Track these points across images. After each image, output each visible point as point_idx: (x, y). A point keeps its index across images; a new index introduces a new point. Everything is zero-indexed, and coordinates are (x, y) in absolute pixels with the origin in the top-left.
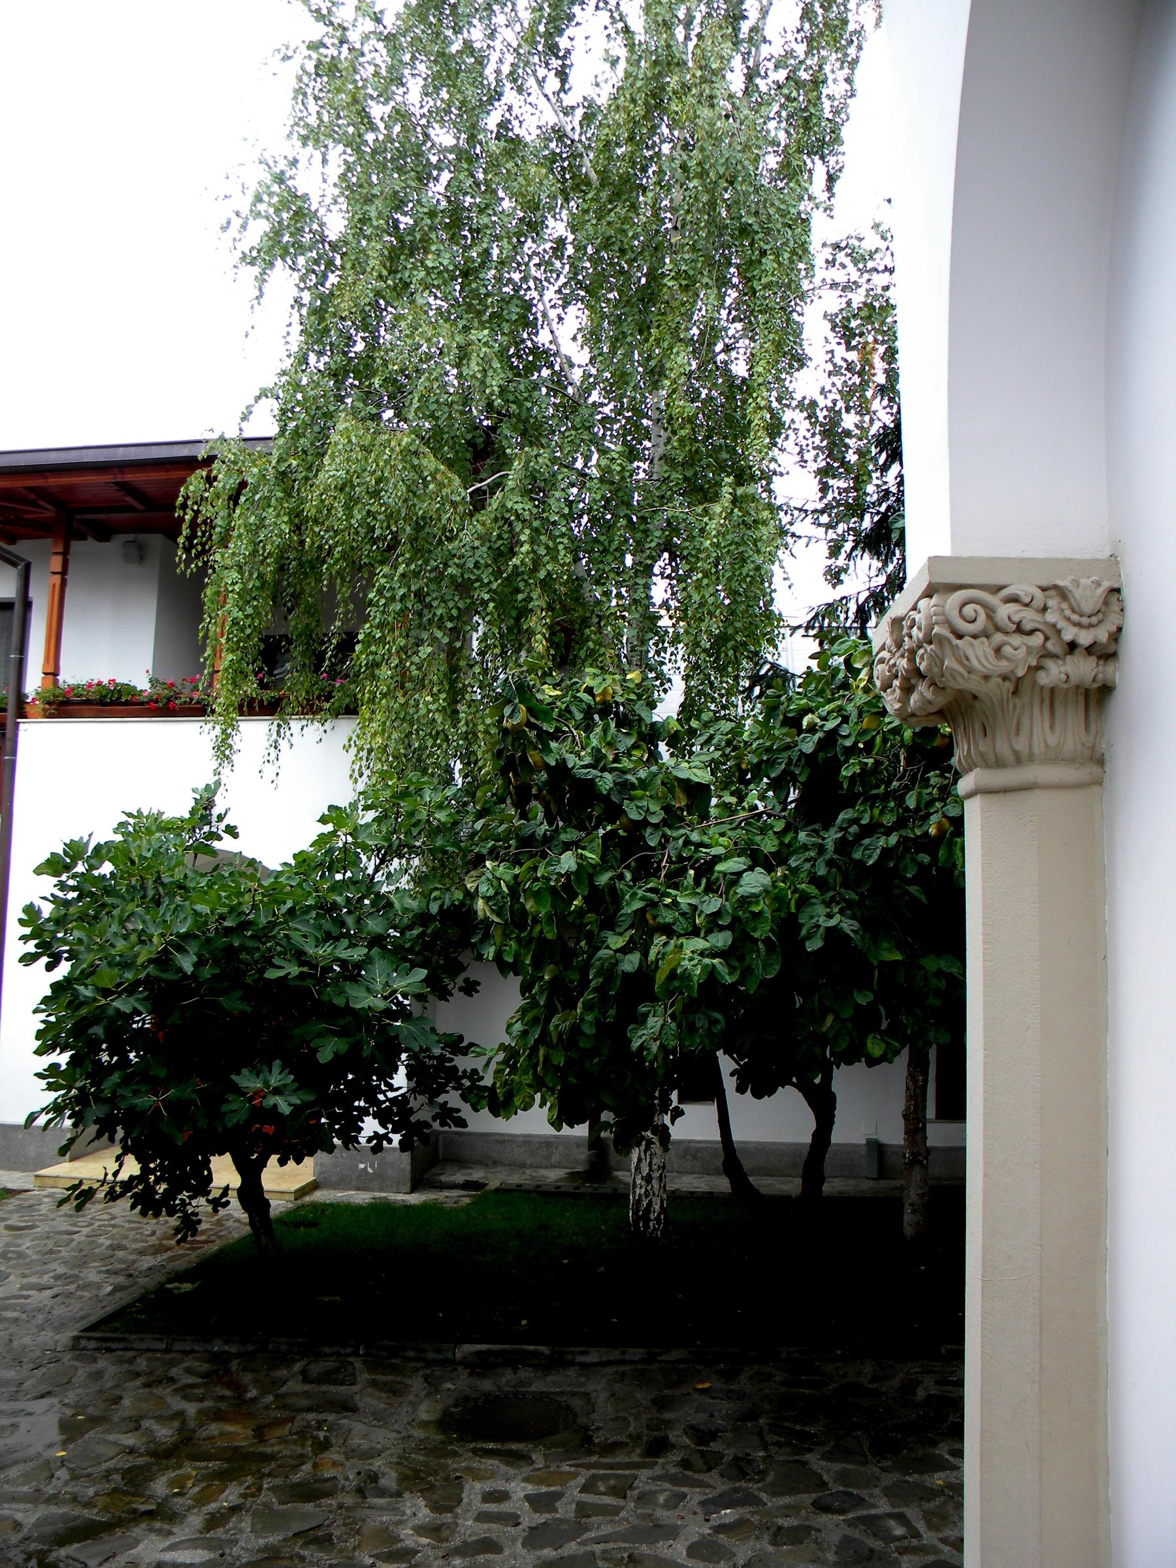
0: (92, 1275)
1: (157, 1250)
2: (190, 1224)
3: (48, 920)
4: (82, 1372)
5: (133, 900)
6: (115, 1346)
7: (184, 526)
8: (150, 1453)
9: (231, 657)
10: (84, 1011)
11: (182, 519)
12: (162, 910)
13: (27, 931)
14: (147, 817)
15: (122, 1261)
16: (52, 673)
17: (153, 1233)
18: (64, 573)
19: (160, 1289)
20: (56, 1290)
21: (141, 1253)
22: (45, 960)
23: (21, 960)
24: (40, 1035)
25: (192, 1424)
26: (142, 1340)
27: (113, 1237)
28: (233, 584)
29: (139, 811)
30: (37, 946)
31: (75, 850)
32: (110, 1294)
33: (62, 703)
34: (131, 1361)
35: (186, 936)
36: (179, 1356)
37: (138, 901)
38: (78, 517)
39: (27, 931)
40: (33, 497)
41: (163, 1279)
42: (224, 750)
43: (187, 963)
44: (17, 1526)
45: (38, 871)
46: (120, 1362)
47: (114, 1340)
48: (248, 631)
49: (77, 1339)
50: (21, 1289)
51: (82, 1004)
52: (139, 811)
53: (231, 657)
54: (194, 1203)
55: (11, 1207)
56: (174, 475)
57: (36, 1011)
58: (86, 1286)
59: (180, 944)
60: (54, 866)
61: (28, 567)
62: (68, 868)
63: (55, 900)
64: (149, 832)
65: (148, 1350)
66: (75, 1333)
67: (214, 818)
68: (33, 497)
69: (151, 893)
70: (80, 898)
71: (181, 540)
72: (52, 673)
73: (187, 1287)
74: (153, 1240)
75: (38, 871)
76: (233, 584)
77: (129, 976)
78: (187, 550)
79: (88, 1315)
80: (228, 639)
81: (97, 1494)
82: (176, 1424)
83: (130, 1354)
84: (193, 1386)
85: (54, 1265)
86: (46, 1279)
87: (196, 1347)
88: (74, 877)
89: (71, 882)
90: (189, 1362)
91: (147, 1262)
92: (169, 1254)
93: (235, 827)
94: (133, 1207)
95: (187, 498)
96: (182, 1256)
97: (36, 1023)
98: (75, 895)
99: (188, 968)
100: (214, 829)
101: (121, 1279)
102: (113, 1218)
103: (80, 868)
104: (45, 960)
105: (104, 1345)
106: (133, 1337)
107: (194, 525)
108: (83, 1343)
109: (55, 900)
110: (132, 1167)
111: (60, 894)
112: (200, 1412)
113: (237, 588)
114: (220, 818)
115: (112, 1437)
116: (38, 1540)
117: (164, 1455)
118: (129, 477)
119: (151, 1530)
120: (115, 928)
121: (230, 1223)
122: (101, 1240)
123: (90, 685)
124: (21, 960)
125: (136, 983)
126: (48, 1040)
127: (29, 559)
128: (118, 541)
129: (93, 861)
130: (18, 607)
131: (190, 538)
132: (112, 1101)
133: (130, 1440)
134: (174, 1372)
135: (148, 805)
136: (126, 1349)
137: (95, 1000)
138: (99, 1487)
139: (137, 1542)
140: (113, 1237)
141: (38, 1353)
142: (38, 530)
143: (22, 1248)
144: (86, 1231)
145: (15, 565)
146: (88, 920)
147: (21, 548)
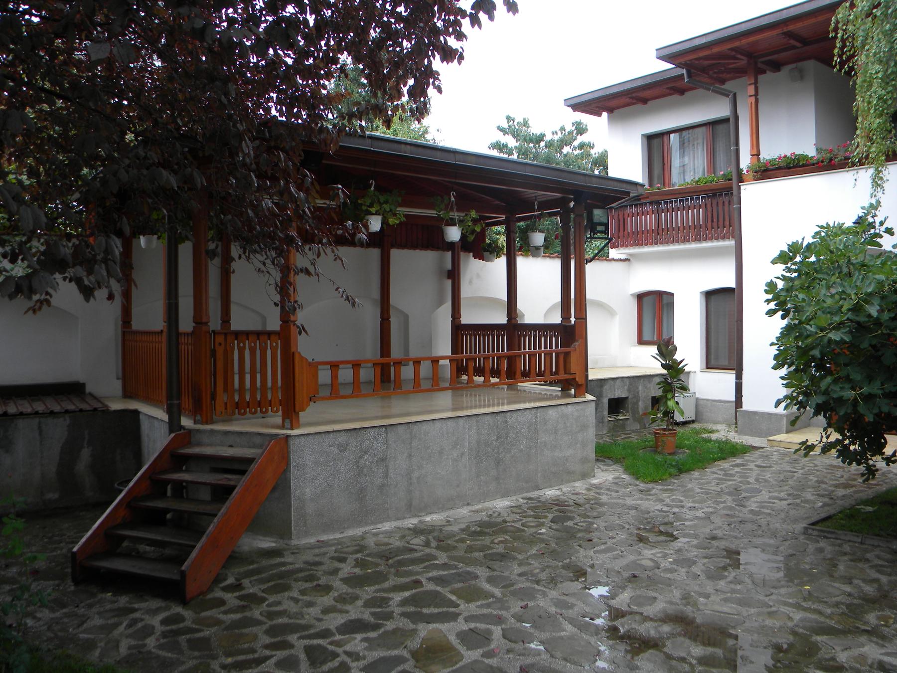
0: (809, 495)
1: (846, 486)
2: (871, 471)
3: (782, 290)
4: (811, 547)
5: (834, 274)
6: (829, 536)
7: (837, 41)
8: (864, 599)
9: (878, 121)
10: (810, 340)
11: (836, 37)
12: (854, 278)
13: (770, 296)
14: (834, 227)
15: (825, 490)
16: (756, 154)
17: (842, 477)
18: (756, 94)
19: (852, 508)
20: (789, 501)
21: (837, 486)
22: (780, 313)
23: (767, 314)
24: (776, 357)
25: (886, 588)
26: (846, 535)
27: (817, 476)
28: (877, 73)
29: (827, 224)
30: (776, 305)
31: (794, 248)
32: (821, 507)
33: (765, 171)
34: (840, 545)
35: (870, 295)
36: (870, 547)
37: (837, 275)
38: (760, 60)
39: (770, 296)
40: (733, 53)
41: (853, 503)
42: (877, 182)
43: (873, 311)
44: (790, 619)
45: (774, 262)
46: (833, 545)
47: (829, 532)
48: (890, 102)
49: (806, 528)
50: (770, 498)
51: (808, 336)
52: (827, 224)
53: (878, 121)
54: (874, 458)
55: (756, 456)
56: (821, 18)
57: (772, 344)
58: (807, 501)
59: (868, 298)
60: (783, 258)
61: (735, 95)
62: (791, 259)
63: (784, 278)
64: (836, 235)
65: (850, 541)
66: (805, 525)
67: (877, 224)
68: (733, 53)
69: (845, 270)
70: (799, 276)
71: (836, 51)
72: (756, 154)
73: (870, 509)
74: (842, 481)
75: (774, 262)
76: (877, 73)
77: (837, 319)
78: (840, 56)
79: (811, 517)
80: (875, 110)
81: (832, 613)
82: (876, 585)
83: (839, 541)
84: (881, 566)
85: (786, 488)
86: (782, 495)
87: (881, 544)
88: (794, 264)
89: (793, 267)
90: (877, 552)
91: (841, 492)
92: (854, 489)
93: (892, 229)
94: (838, 457)
95: (837, 22)
96: (862, 491)
97: (774, 351)
98: (796, 274)
99: (874, 313)
100: (877, 231)
101: (826, 500)
102: (816, 466)
103: (798, 259)
104: (780, 313)
105: (823, 534)
106: (840, 532)
107: (843, 41)
108: (810, 531)
109: (784, 278)
110: (835, 436)
111: (788, 275)
112: (890, 582)
113: (880, 75)
114: (882, 223)
115: (836, 585)
116: (804, 628)
117: (871, 602)
118: (791, 28)
119: (871, 641)
120: (823, 291)
121: (891, 475)
122: (811, 477)
123: (780, 158)
124: (767, 314)
125: (842, 323)
126: (780, 361)
127: (735, 91)
128: (786, 70)
129: (806, 254)
130: (732, 120)
131: (842, 48)
132: (826, 392)
133: (848, 588)
134: (868, 556)
135: (832, 219)
136: (837, 539)
137: (816, 333)
138: (833, 610)
139: (863, 646)
140: (817, 476)
141: (784, 533)
142: (740, 72)
143: (766, 477)
144: (801, 471)
145: (727, 96)
146: (807, 288)
147: (728, 86)
